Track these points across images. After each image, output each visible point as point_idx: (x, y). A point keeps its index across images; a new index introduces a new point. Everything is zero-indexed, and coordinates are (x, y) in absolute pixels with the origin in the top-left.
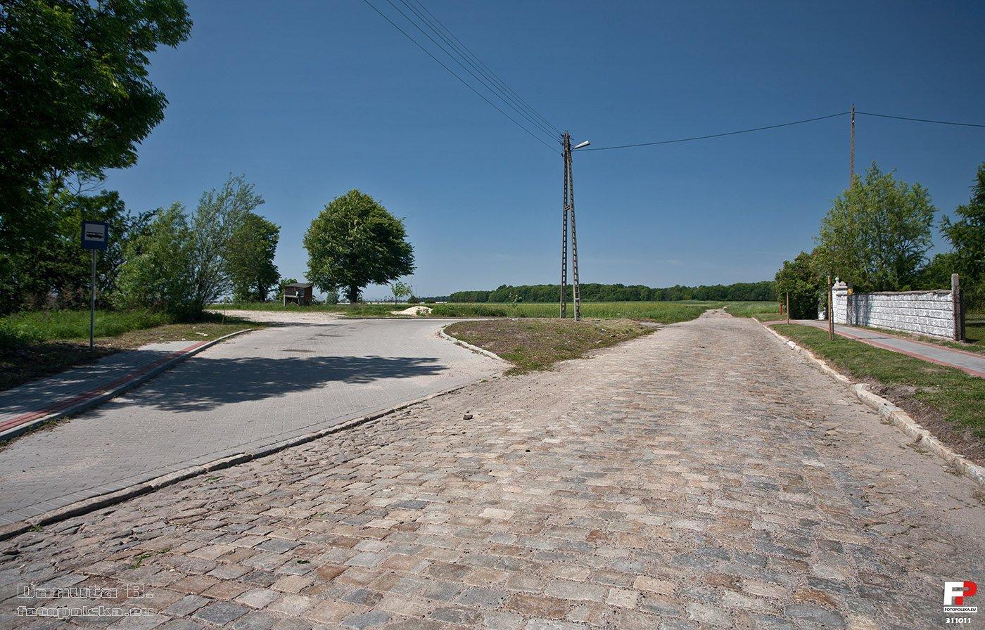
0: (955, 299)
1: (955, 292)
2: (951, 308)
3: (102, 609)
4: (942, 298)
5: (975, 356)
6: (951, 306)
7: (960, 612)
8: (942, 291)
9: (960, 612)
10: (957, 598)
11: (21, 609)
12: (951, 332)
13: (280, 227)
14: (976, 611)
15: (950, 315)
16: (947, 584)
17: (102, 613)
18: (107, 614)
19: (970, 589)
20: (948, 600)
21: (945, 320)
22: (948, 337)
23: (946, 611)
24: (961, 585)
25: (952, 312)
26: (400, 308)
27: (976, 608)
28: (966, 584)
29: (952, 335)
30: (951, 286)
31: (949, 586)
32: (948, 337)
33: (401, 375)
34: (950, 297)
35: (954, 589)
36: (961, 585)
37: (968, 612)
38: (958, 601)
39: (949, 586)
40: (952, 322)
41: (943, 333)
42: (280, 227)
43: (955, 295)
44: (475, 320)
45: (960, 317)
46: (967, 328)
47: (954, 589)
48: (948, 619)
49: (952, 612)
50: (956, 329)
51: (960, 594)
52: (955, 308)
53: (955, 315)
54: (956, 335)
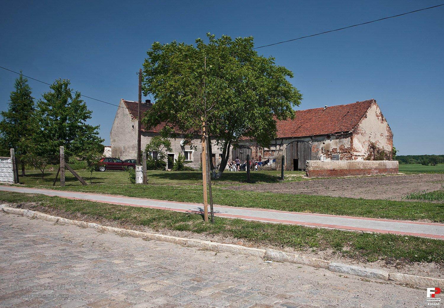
0: (13, 162)
1: (13, 158)
2: (11, 167)
4: (4, 161)
5: (406, 222)
6: (11, 165)
7: (434, 300)
8: (4, 158)
10: (432, 294)
12: (11, 179)
15: (11, 170)
16: (428, 289)
19: (438, 291)
20: (428, 296)
21: (7, 173)
22: (9, 182)
24: (434, 289)
25: (11, 169)
26: (69, 179)
28: (436, 288)
29: (12, 181)
30: (10, 155)
31: (429, 289)
32: (9, 182)
34: (10, 161)
35: (431, 291)
38: (433, 296)
40: (12, 174)
41: (6, 180)
43: (13, 160)
45: (15, 171)
46: (20, 178)
47: (431, 291)
48: (429, 303)
50: (15, 177)
51: (434, 293)
52: (14, 166)
53: (14, 170)
54: (15, 181)
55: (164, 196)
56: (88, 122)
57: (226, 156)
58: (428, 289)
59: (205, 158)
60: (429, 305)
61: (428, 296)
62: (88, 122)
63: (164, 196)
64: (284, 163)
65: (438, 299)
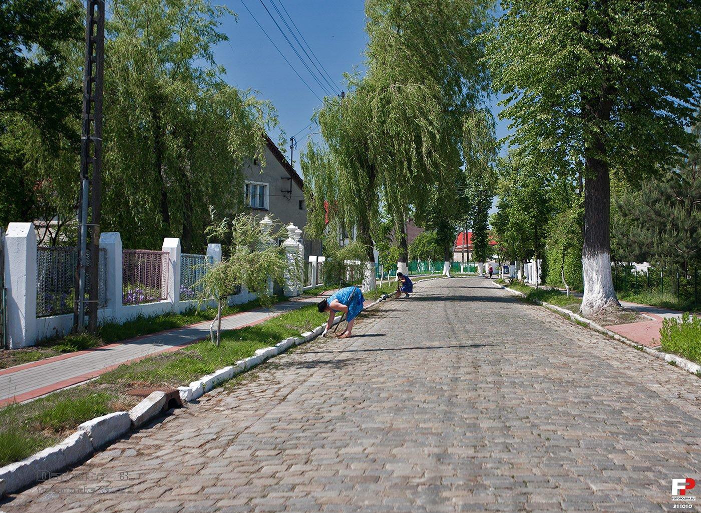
16: (674, 480)
19: (691, 484)
20: (675, 492)
24: (684, 481)
35: (679, 484)
38: (682, 492)
47: (679, 484)
48: (675, 505)
51: (683, 487)
55: (160, 244)
56: (64, 84)
57: (39, 455)
58: (674, 480)
59: (365, 352)
60: (675, 507)
61: (675, 492)
62: (64, 84)
63: (160, 244)
64: (9, 265)
65: (690, 497)
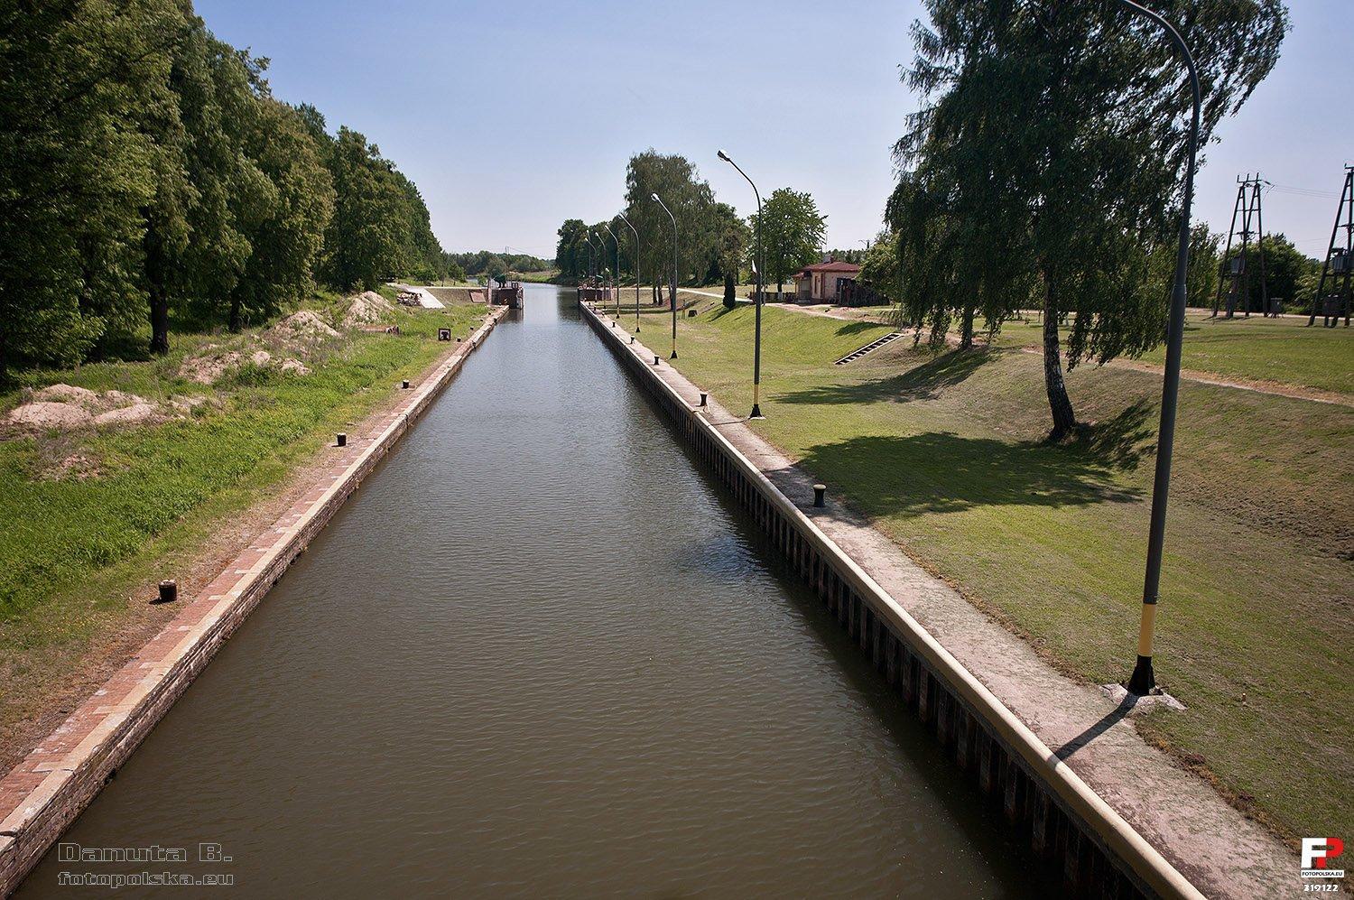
3: (167, 876)
9: (1323, 876)
11: (63, 876)
13: (825, 217)
14: (1343, 876)
17: (167, 881)
18: (174, 882)
23: (1304, 876)
27: (1343, 871)
31: (1307, 843)
33: (919, 506)
35: (1316, 848)
36: (1322, 842)
37: (1332, 876)
39: (1307, 843)
42: (825, 217)
44: (784, 498)
47: (1316, 848)
48: (1307, 886)
49: (1312, 876)
51: (1322, 854)
